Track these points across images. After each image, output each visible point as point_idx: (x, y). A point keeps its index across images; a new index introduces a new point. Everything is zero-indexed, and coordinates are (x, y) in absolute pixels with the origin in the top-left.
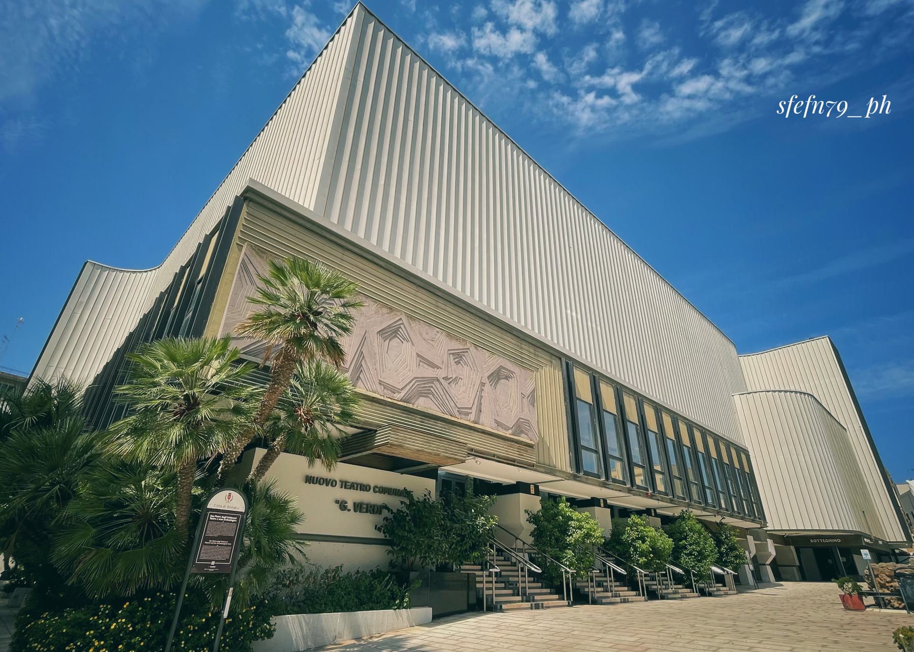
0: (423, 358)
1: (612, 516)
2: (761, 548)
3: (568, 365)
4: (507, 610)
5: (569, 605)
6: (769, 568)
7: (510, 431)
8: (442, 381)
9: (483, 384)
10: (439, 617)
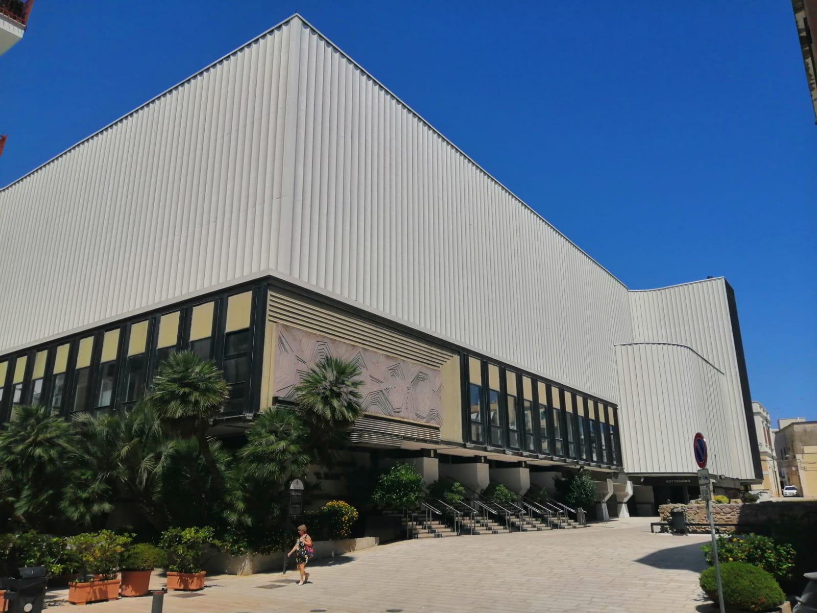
0: (373, 378)
1: (490, 467)
2: (621, 488)
3: (464, 354)
4: (169, 575)
5: (457, 535)
6: (604, 506)
7: (425, 420)
8: (384, 392)
9: (408, 388)
10: (382, 542)
